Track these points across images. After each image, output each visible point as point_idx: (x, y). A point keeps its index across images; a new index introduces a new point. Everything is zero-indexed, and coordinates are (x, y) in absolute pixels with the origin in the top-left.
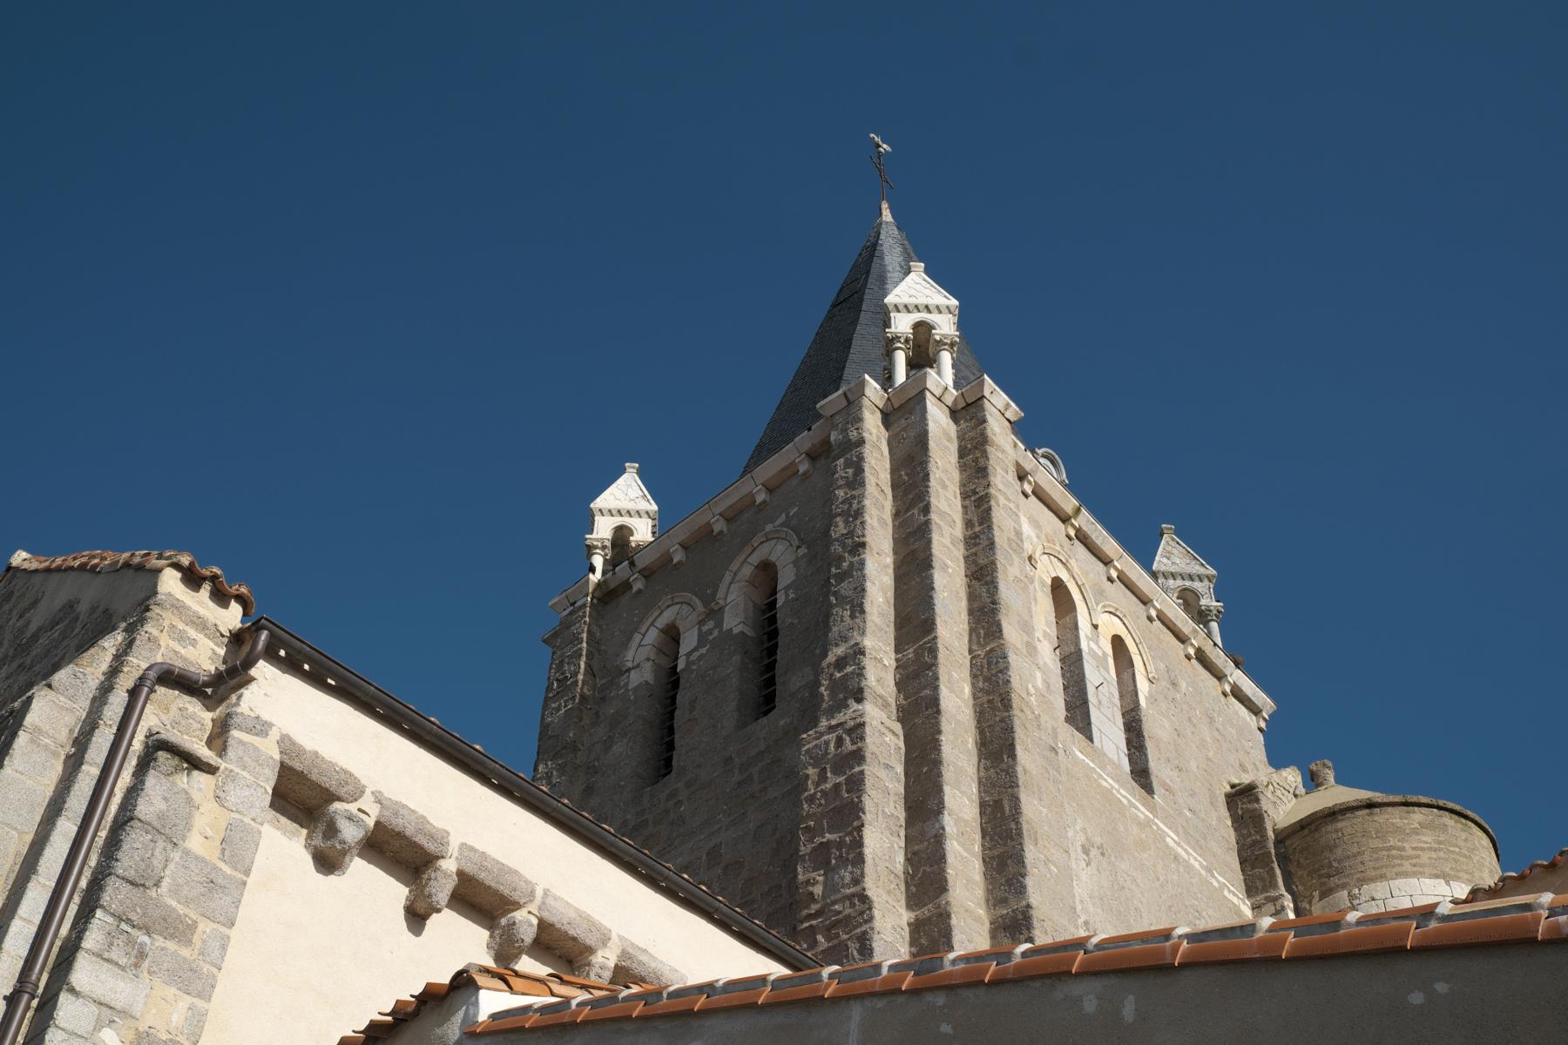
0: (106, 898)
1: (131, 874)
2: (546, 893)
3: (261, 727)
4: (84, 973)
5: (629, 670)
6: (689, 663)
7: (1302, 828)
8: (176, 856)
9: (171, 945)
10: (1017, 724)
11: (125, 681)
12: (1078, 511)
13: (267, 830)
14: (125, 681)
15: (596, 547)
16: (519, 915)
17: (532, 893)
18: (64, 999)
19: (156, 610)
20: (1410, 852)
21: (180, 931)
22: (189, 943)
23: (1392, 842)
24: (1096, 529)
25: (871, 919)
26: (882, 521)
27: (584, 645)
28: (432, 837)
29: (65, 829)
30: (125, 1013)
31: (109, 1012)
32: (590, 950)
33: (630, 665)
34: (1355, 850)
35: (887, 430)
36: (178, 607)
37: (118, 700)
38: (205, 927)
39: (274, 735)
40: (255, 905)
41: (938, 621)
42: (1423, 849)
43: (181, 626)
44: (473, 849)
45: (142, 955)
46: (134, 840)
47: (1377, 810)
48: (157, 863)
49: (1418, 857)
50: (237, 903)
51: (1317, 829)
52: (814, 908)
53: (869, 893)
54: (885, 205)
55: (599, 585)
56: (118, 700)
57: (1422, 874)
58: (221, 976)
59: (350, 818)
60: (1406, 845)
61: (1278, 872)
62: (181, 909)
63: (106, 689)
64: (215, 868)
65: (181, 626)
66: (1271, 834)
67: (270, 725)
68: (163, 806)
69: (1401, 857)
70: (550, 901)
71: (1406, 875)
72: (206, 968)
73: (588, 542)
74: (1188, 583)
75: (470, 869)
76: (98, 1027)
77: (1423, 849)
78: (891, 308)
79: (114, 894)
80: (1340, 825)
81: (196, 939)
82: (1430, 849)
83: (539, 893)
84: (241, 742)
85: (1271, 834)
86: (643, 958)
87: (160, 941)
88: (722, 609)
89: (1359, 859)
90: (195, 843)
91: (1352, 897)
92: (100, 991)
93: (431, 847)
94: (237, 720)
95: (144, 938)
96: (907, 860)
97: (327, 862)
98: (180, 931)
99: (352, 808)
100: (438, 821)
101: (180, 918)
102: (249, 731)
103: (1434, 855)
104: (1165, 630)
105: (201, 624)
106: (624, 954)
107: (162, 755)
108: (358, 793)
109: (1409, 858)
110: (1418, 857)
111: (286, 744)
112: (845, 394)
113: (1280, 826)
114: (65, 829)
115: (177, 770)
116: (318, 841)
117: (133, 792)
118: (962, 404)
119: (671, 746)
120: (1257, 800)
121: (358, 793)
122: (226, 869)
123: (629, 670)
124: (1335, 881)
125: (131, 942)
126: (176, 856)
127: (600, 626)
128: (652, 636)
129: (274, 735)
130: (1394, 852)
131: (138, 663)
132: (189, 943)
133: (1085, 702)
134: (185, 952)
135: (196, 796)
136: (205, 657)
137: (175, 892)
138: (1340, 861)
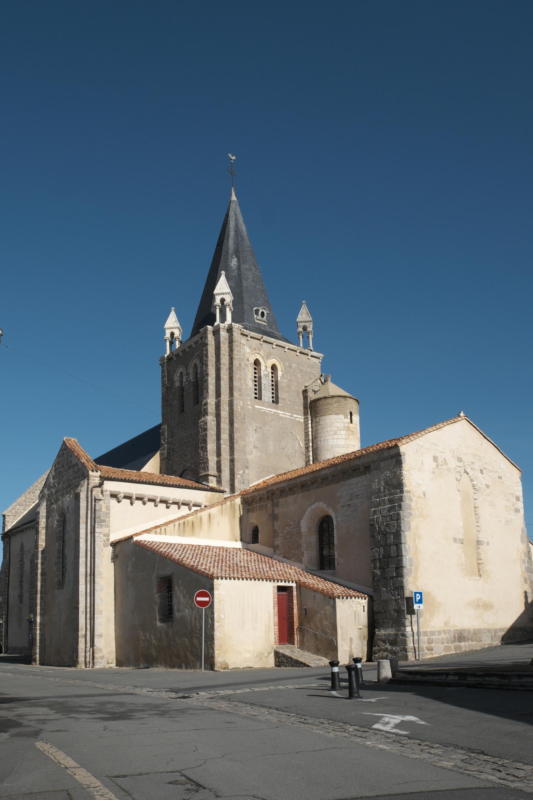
0: (96, 521)
1: (98, 517)
2: (148, 495)
3: (106, 491)
4: (97, 530)
5: (175, 382)
6: (185, 385)
7: (314, 401)
8: (102, 513)
9: (104, 523)
10: (235, 418)
11: (90, 490)
12: (262, 337)
13: (111, 500)
14: (90, 490)
15: (167, 340)
16: (145, 499)
17: (146, 496)
18: (96, 533)
19: (90, 478)
20: (331, 409)
21: (104, 521)
22: (106, 522)
23: (328, 407)
24: (268, 339)
25: (208, 463)
26: (212, 365)
27: (166, 374)
28: (131, 495)
29: (89, 512)
30: (102, 533)
31: (100, 533)
32: (156, 500)
33: (175, 381)
34: (321, 408)
35: (214, 336)
36: (92, 476)
37: (90, 493)
38: (107, 519)
39: (108, 491)
40: (112, 511)
41: (222, 394)
42: (334, 408)
43: (93, 478)
44: (137, 494)
45: (102, 526)
46: (97, 513)
47: (327, 399)
48: (100, 514)
49: (333, 410)
50: (110, 515)
51: (316, 402)
52: (202, 458)
53: (208, 458)
54: (233, 189)
55: (168, 357)
56: (90, 493)
57: (333, 414)
58: (110, 504)
59: (120, 497)
60: (331, 407)
61: (309, 411)
62: (104, 519)
63: (88, 491)
64: (106, 512)
65: (93, 478)
66: (309, 402)
67: (107, 490)
68: (98, 507)
69: (329, 410)
70: (149, 496)
71: (330, 414)
72: (108, 524)
73: (165, 339)
74: (305, 324)
75: (137, 496)
76: (100, 535)
77: (334, 408)
78: (215, 295)
79: (97, 520)
80: (320, 402)
81: (107, 521)
82: (336, 408)
83: (147, 496)
84: (105, 494)
85: (309, 402)
86: (163, 498)
87: (103, 523)
88: (189, 373)
89: (322, 411)
90: (103, 510)
91: (319, 419)
92: (99, 531)
93: (131, 496)
94: (103, 491)
95: (101, 524)
96: (216, 448)
97: (119, 502)
98: (104, 521)
99: (120, 495)
100: (131, 492)
101: (104, 520)
102: (106, 492)
103: (336, 409)
104: (291, 351)
105: (96, 477)
106: (161, 498)
107: (97, 500)
108: (120, 493)
109: (331, 410)
110: (333, 410)
111: (110, 491)
112: (204, 329)
113: (312, 399)
114: (89, 512)
115: (99, 501)
116: (117, 500)
117: (95, 505)
118: (229, 329)
119: (183, 406)
120: (307, 393)
121: (120, 493)
122: (107, 511)
123: (175, 382)
124: (317, 415)
125: (100, 525)
126: (102, 513)
127: (169, 367)
128: (178, 374)
129: (108, 491)
130: (328, 409)
131: (90, 487)
132: (106, 522)
133: (261, 390)
134: (106, 523)
135: (102, 504)
136: (97, 481)
137: (103, 517)
138: (318, 411)
